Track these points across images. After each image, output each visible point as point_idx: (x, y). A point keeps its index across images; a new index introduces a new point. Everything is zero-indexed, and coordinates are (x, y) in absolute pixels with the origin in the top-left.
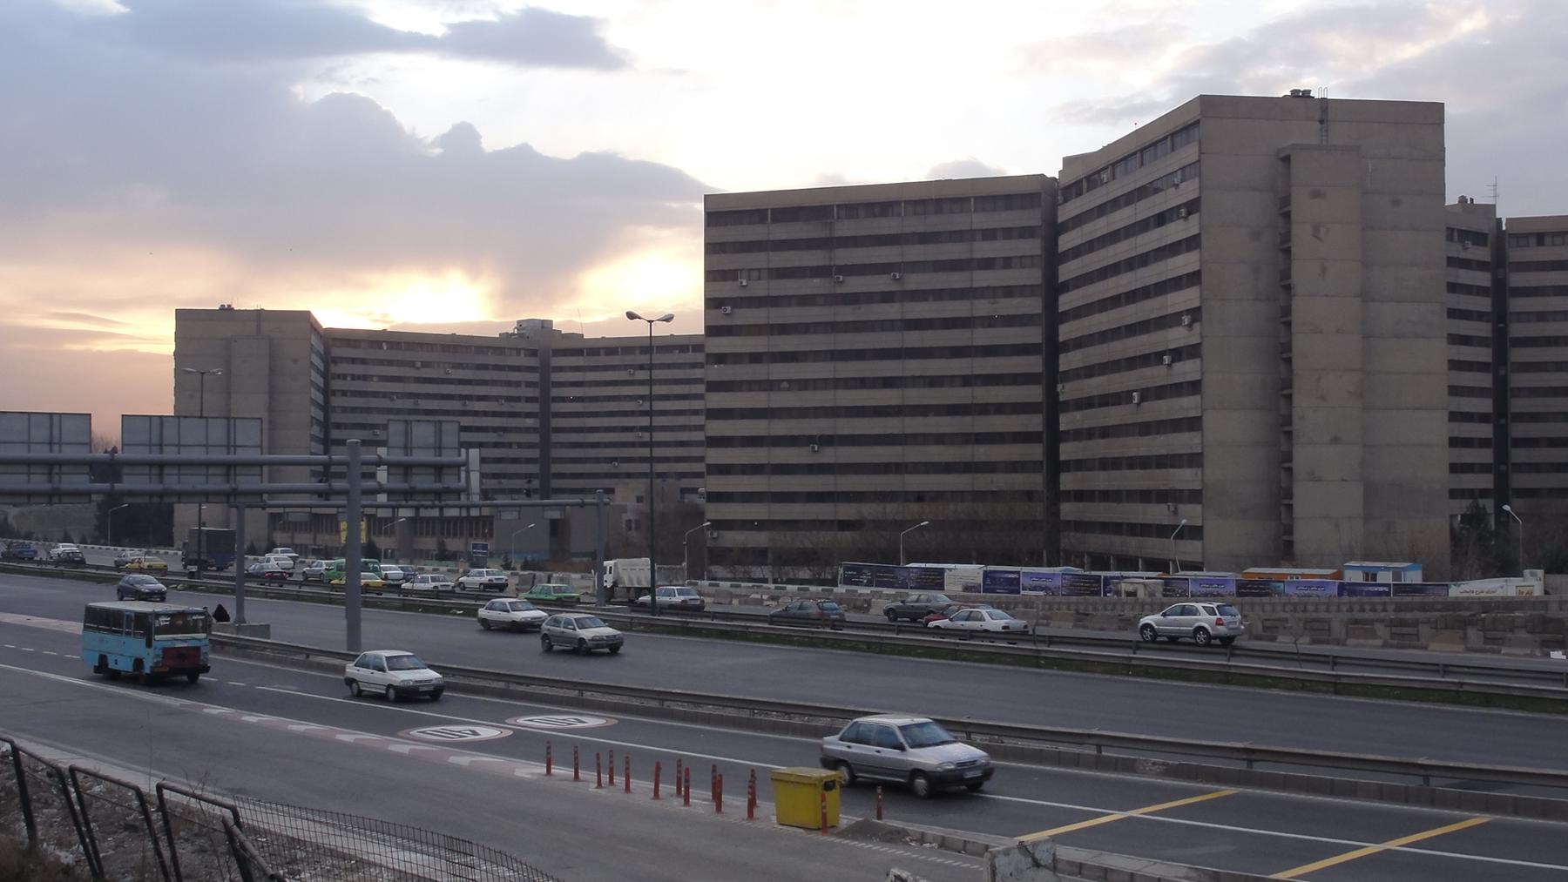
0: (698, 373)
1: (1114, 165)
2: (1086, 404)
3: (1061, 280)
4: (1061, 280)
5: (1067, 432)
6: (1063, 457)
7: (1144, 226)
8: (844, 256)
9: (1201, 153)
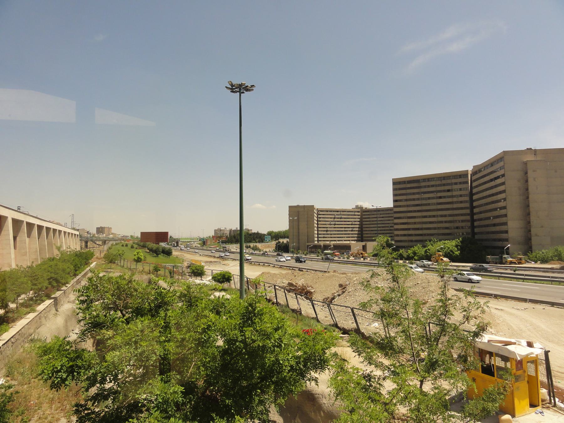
0: (392, 215)
1: (484, 167)
2: (480, 220)
3: (473, 192)
4: (473, 192)
5: (476, 226)
6: (475, 219)
7: (491, 180)
8: (423, 190)
9: (504, 163)
